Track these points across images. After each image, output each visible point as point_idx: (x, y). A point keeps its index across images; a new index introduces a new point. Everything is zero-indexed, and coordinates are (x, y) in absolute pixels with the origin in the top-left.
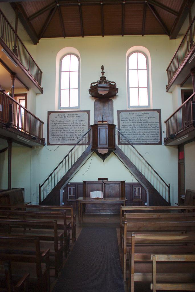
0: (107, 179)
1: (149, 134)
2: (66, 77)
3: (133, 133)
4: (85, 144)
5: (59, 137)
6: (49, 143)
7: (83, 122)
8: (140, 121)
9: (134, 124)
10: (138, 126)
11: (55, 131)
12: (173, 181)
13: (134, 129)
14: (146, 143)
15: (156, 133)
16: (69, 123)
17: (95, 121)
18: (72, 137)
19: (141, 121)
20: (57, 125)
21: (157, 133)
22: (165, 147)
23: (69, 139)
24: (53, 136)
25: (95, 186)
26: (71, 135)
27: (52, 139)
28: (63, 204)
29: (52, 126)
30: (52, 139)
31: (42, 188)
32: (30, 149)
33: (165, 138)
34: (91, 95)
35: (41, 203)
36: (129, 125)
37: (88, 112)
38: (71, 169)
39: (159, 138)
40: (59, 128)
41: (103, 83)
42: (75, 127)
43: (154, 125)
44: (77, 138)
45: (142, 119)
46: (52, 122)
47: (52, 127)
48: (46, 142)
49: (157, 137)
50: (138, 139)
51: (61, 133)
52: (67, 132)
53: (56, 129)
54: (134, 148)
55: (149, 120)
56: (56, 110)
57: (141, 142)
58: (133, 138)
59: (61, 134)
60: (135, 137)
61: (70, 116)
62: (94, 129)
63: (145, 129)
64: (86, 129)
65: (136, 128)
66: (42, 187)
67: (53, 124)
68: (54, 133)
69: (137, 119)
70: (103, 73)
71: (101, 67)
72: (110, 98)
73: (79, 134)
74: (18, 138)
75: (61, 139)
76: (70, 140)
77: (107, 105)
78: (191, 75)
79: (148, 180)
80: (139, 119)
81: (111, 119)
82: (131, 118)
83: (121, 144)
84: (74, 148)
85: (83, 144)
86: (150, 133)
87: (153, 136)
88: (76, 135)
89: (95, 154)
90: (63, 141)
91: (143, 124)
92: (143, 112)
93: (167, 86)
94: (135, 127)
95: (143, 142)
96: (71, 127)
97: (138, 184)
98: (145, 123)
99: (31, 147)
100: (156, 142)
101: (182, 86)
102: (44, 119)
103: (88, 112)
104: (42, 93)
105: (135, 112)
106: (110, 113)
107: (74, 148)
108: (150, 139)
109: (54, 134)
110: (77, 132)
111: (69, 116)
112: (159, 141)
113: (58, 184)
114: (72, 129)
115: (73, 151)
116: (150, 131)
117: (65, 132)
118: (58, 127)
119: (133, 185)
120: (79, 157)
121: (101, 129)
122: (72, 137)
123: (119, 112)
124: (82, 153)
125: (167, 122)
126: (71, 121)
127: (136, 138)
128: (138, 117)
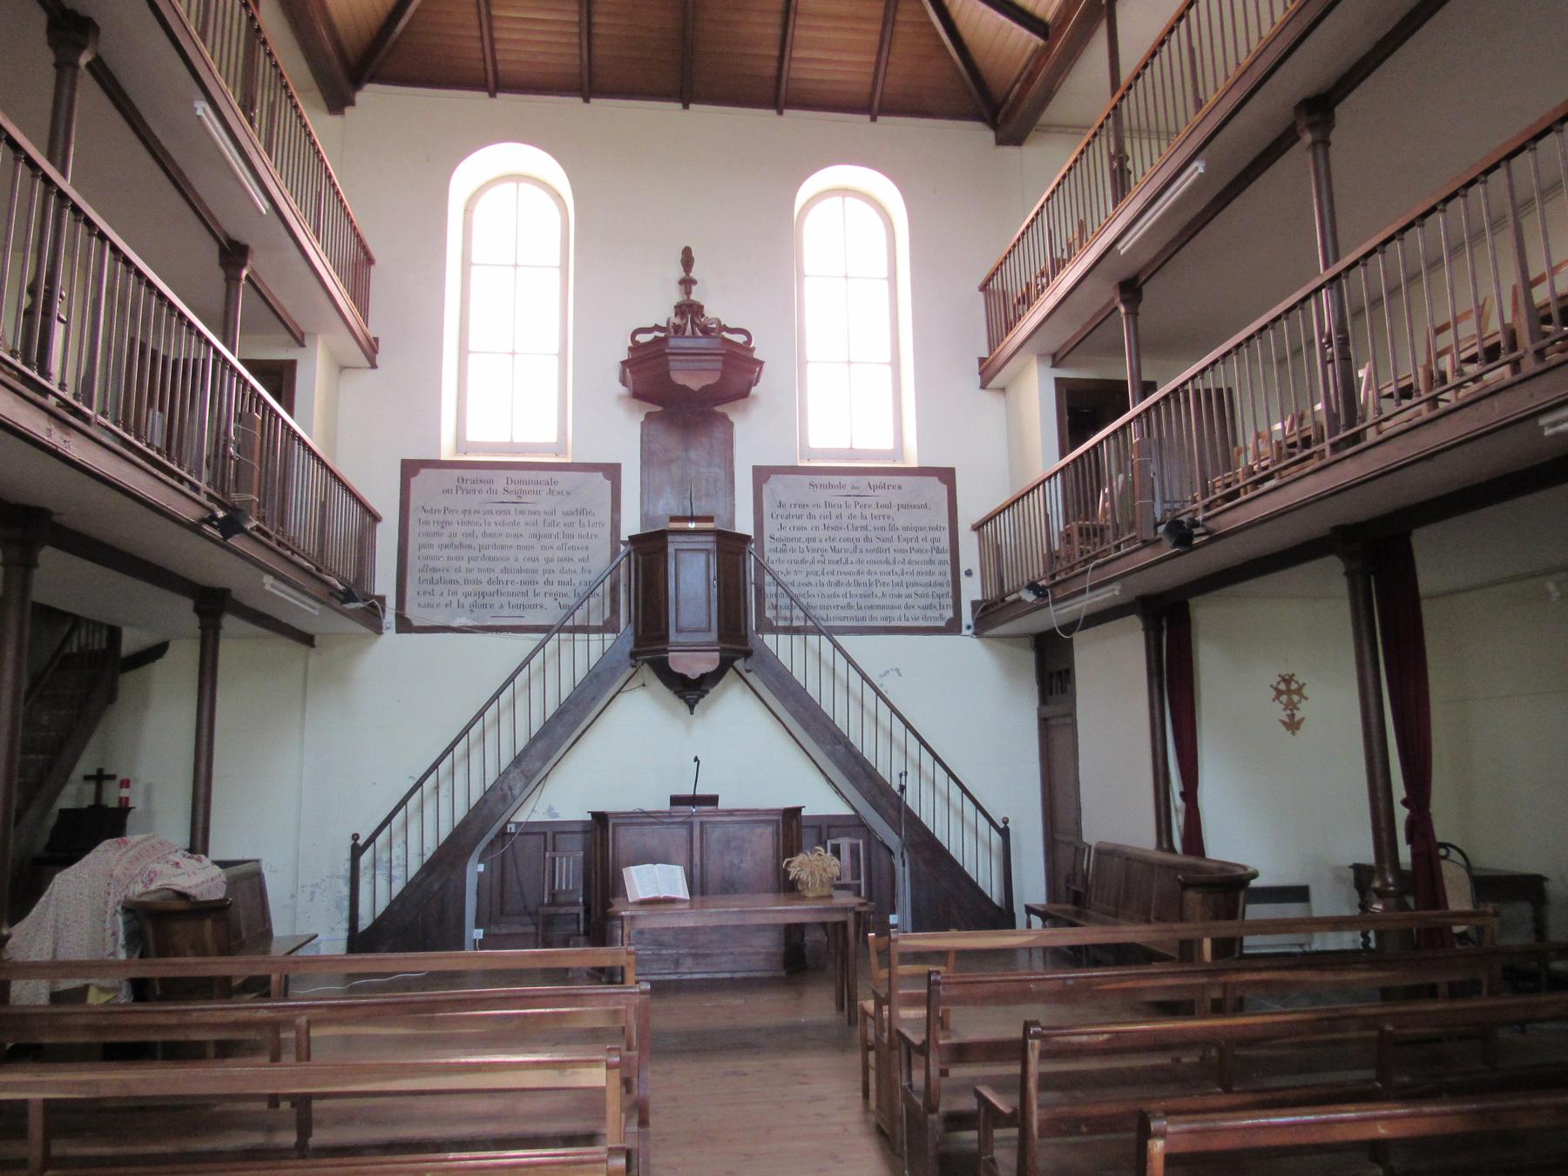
0: (713, 800)
1: (900, 584)
2: (491, 292)
3: (825, 579)
4: (597, 630)
5: (462, 589)
6: (408, 621)
7: (585, 519)
8: (858, 522)
9: (832, 534)
10: (850, 546)
11: (438, 558)
12: (1017, 796)
13: (830, 556)
14: (887, 624)
15: (933, 579)
16: (514, 523)
17: (645, 518)
18: (531, 593)
19: (864, 523)
20: (449, 529)
21: (940, 579)
22: (976, 642)
23: (515, 600)
24: (429, 588)
25: (652, 837)
26: (523, 583)
27: (423, 600)
28: (479, 934)
29: (427, 534)
30: (423, 600)
31: (365, 859)
32: (299, 649)
33: (975, 604)
34: (623, 390)
35: (359, 941)
36: (808, 540)
37: (612, 472)
38: (525, 751)
39: (950, 601)
40: (461, 546)
41: (689, 331)
42: (545, 542)
43: (925, 539)
44: (556, 596)
45: (867, 512)
46: (423, 516)
47: (424, 540)
48: (389, 618)
49: (940, 596)
50: (849, 607)
51: (469, 571)
52: (501, 565)
53: (446, 552)
54: (836, 646)
55: (901, 519)
56: (446, 454)
57: (864, 619)
58: (825, 602)
59: (472, 576)
60: (835, 595)
61: (518, 487)
62: (649, 552)
63: (882, 557)
64: (599, 556)
65: (839, 551)
66: (370, 850)
67: (427, 523)
68: (435, 570)
69: (845, 512)
70: (687, 283)
71: (680, 256)
72: (719, 409)
73: (566, 578)
74: (268, 587)
75: (470, 600)
76: (518, 606)
77: (704, 439)
78: (1116, 308)
79: (900, 799)
80: (857, 512)
81: (719, 510)
82: (818, 506)
83: (776, 630)
84: (542, 645)
85: (585, 629)
86: (906, 578)
87: (920, 590)
88: (548, 582)
89: (647, 673)
90: (484, 611)
91: (871, 535)
92: (875, 480)
93: (982, 361)
94: (834, 550)
95: (872, 618)
96: (523, 542)
97: (853, 825)
98: (883, 529)
99: (308, 640)
100: (936, 619)
101: (1057, 360)
102: (383, 497)
103: (612, 472)
104: (374, 366)
105: (834, 479)
106: (716, 481)
107: (542, 645)
108: (907, 607)
109: (437, 576)
110: (554, 565)
111: (511, 487)
112: (949, 614)
113: (458, 833)
114: (529, 553)
115: (536, 662)
116: (908, 568)
117: (491, 565)
118: (457, 541)
119: (829, 827)
120: (566, 691)
121: (682, 556)
122: (531, 593)
123: (761, 475)
124: (581, 674)
125: (990, 527)
126: (522, 512)
127: (843, 602)
128: (851, 501)
